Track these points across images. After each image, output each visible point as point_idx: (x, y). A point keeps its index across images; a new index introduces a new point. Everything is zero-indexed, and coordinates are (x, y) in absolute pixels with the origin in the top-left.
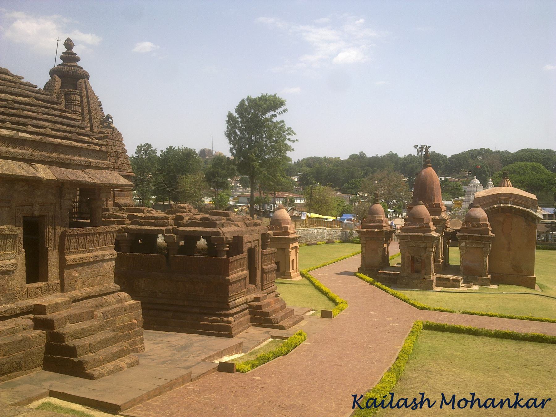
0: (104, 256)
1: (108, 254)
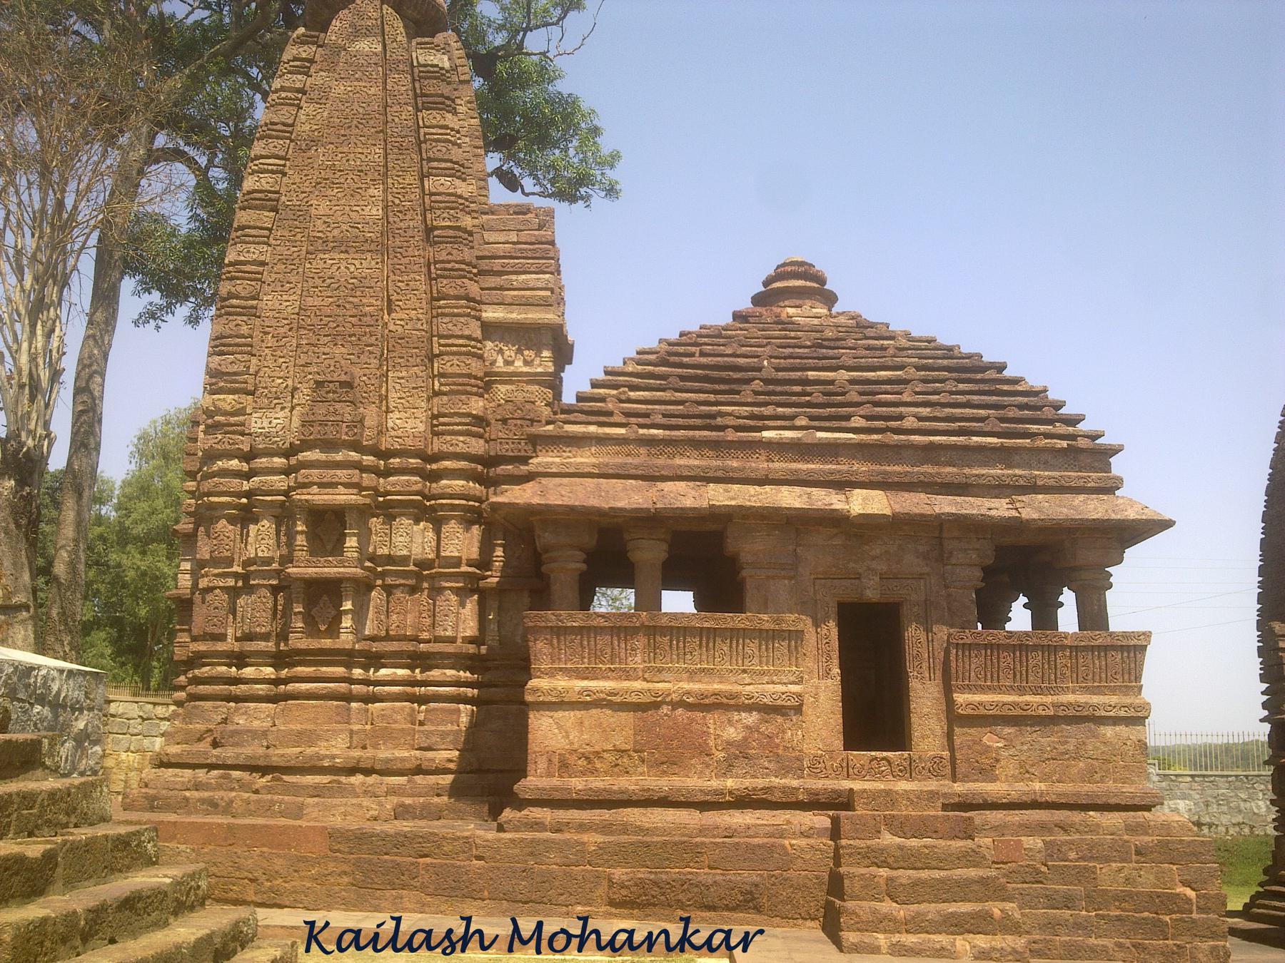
0: (1095, 707)
1: (1112, 704)
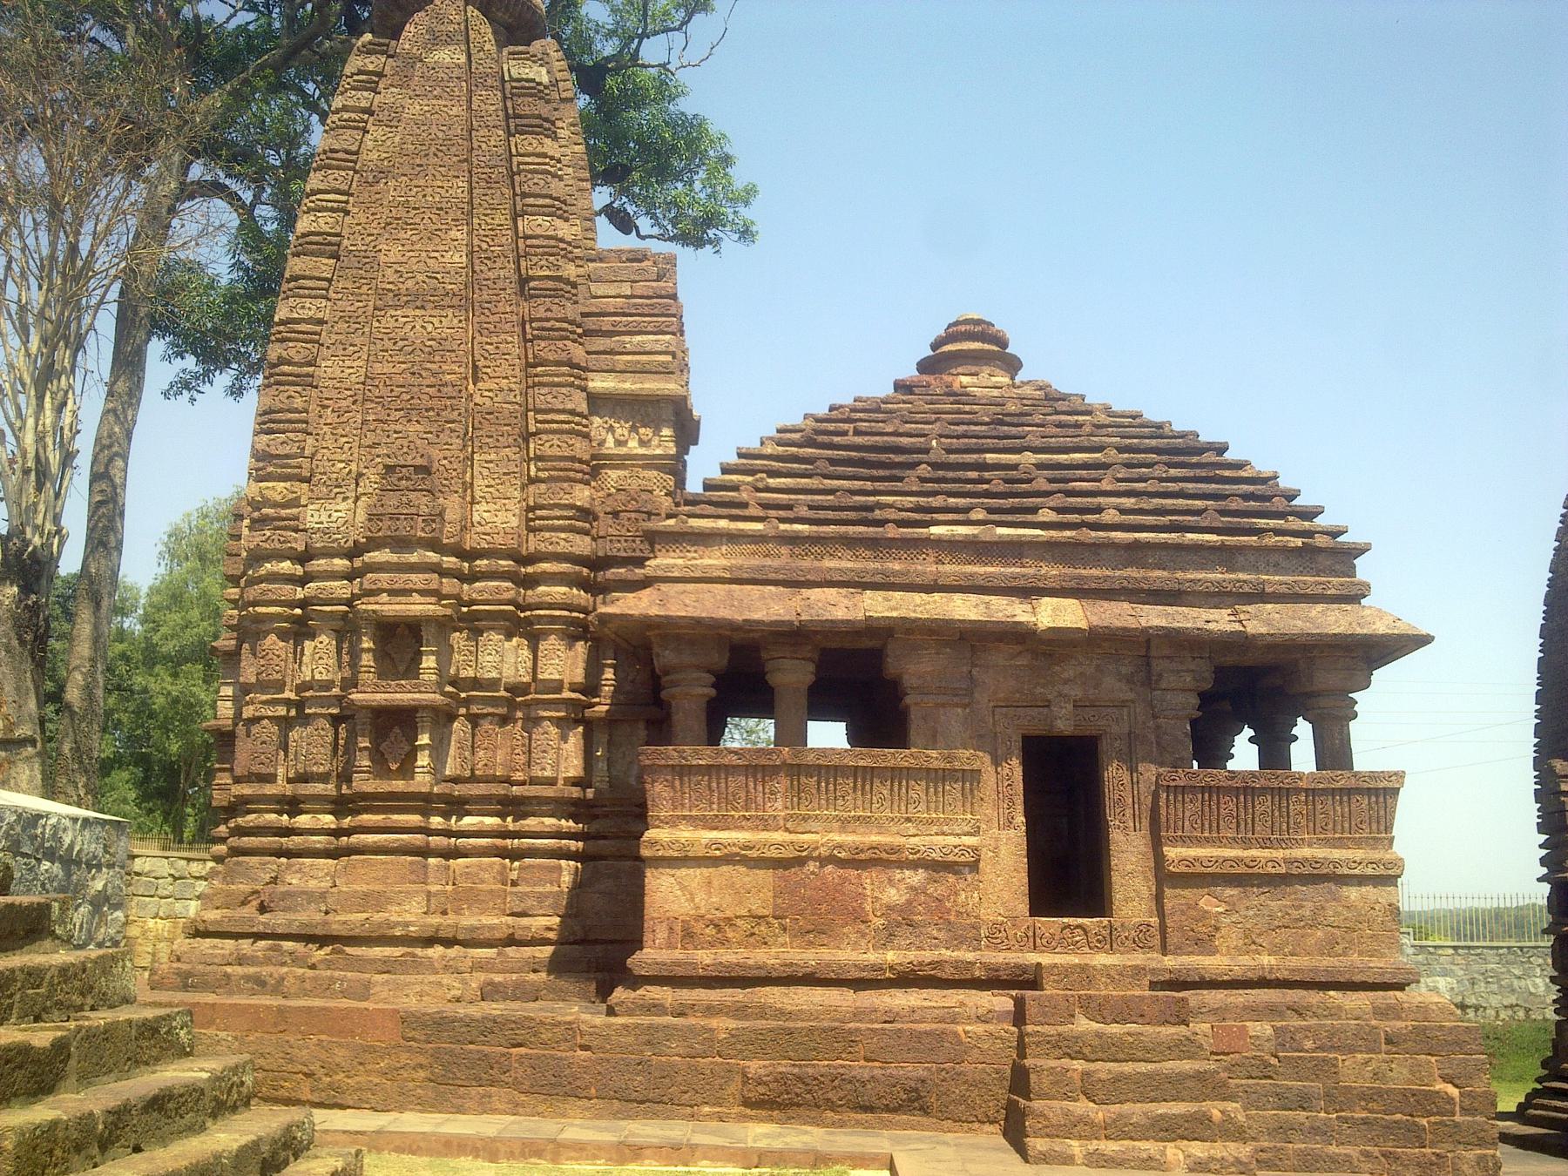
0: (1336, 863)
